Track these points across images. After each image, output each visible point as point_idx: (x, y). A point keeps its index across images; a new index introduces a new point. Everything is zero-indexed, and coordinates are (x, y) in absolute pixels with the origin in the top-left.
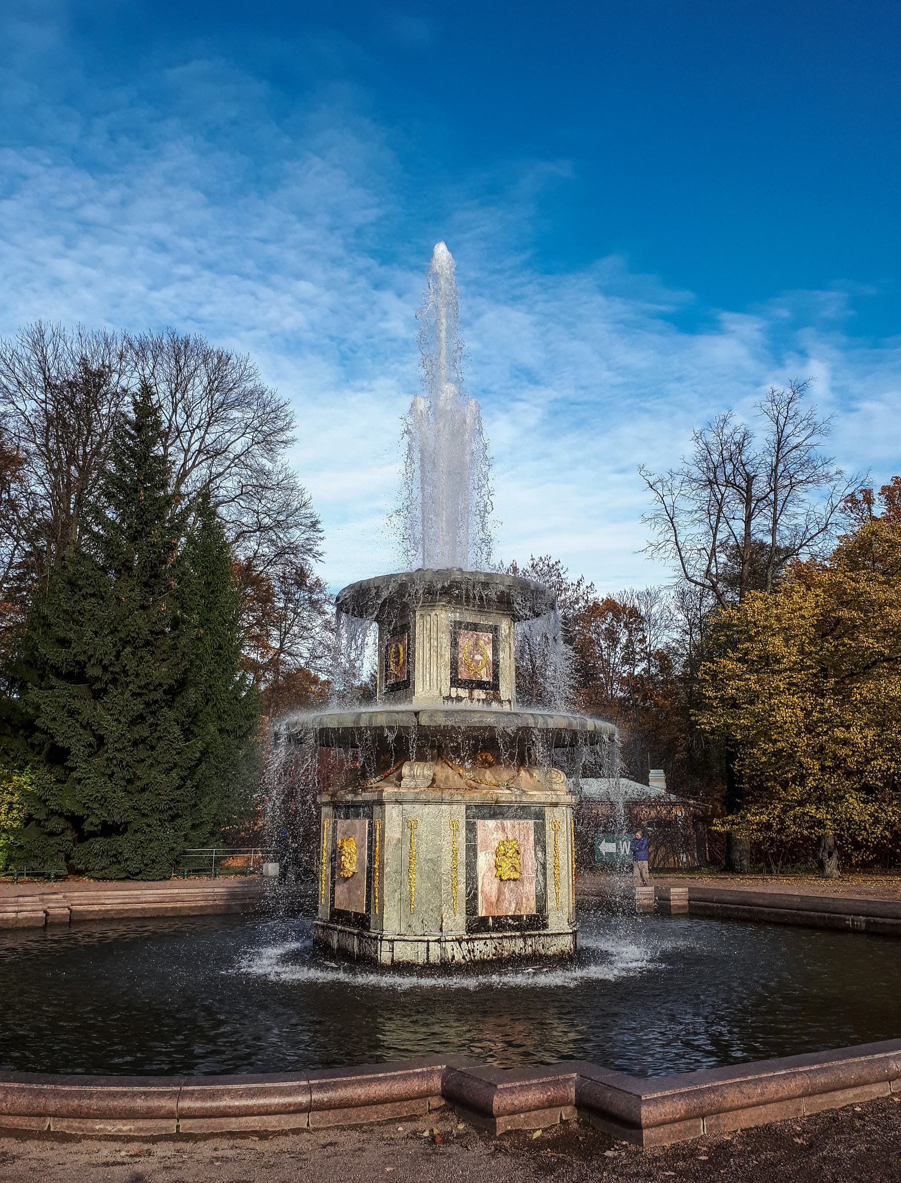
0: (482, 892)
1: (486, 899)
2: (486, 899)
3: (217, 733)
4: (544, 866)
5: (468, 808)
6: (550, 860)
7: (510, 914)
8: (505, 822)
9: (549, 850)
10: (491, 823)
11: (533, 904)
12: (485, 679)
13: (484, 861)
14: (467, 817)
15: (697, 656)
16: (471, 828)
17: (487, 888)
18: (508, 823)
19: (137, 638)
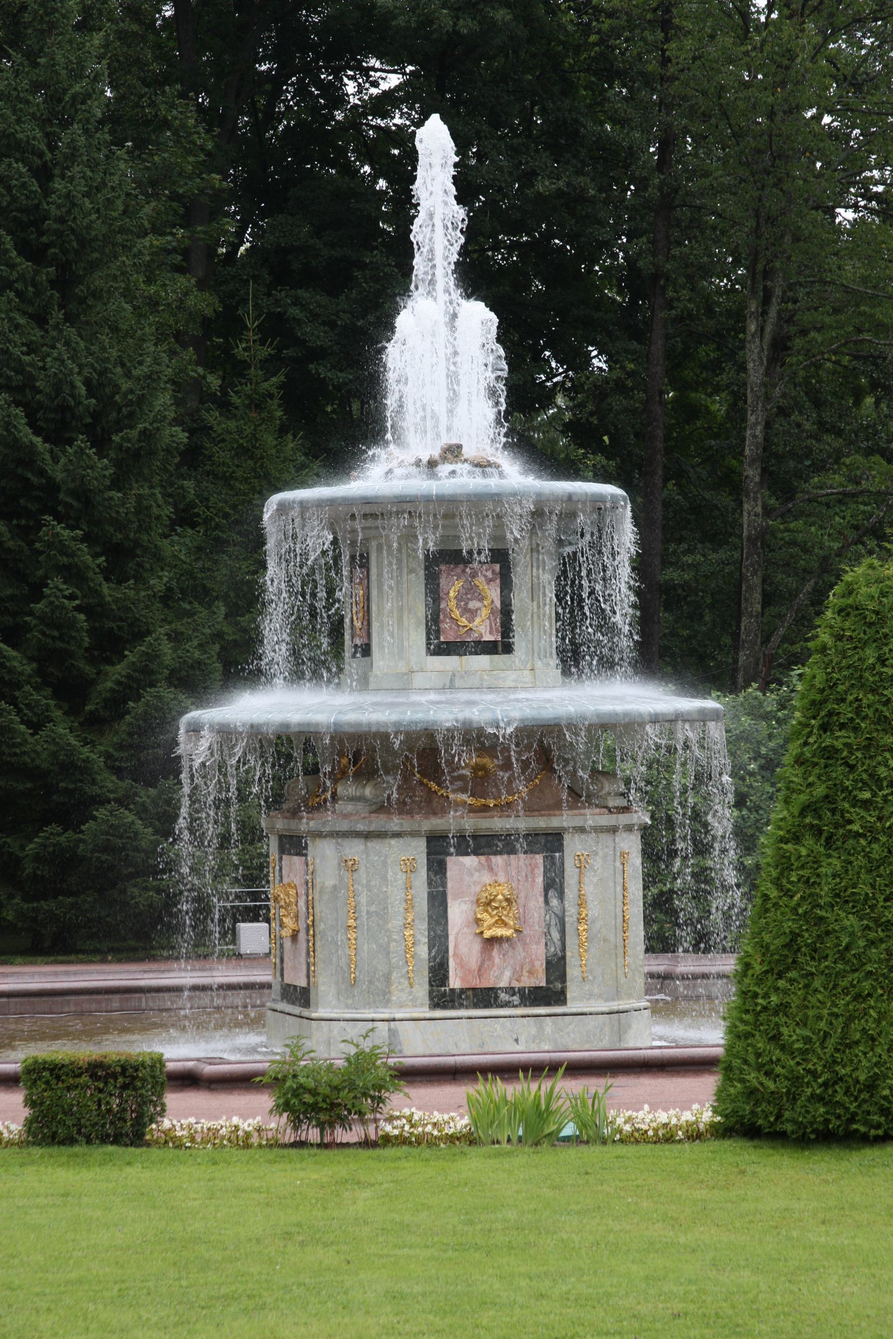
0: (455, 955)
1: (461, 965)
6: (571, 911)
7: (503, 984)
8: (493, 858)
9: (570, 893)
11: (540, 966)
12: (487, 638)
17: (463, 950)
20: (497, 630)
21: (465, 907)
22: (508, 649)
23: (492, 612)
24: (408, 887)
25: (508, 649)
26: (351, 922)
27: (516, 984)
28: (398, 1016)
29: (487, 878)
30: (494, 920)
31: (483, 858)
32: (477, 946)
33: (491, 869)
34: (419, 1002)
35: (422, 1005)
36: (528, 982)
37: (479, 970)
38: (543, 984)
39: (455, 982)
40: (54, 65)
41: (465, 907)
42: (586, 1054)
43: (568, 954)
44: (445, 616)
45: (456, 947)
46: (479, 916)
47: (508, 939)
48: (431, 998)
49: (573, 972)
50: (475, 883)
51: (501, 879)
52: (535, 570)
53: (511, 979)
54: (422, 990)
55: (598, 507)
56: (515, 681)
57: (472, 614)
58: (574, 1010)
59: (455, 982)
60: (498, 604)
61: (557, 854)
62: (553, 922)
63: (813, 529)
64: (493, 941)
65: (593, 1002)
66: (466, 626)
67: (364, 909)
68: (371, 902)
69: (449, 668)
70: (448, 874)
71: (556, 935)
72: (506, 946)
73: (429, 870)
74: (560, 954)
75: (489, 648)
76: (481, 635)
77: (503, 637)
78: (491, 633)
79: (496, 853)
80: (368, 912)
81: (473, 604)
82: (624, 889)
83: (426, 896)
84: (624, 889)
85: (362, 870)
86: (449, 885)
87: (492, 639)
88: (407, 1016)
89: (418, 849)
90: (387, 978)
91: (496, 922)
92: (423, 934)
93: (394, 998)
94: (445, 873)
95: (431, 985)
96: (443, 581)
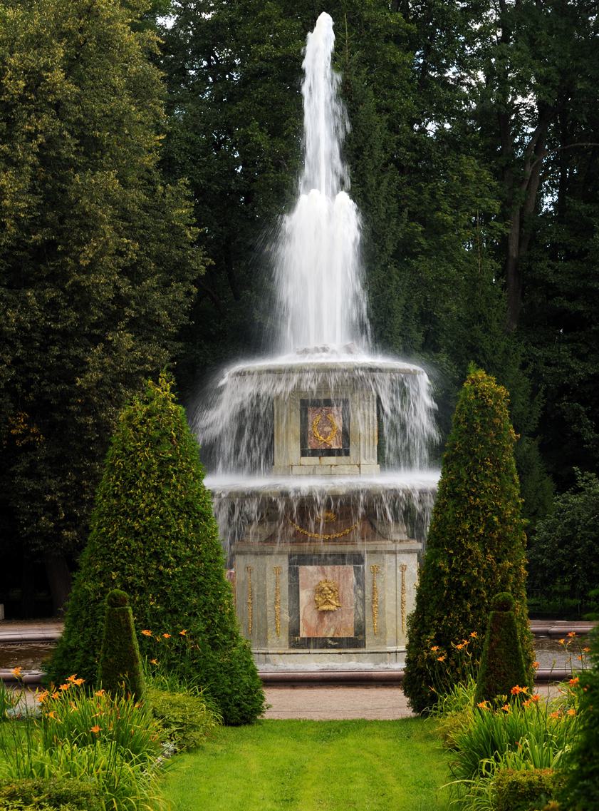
0: (303, 619)
1: (306, 624)
2: (306, 624)
3: (503, 349)
4: (363, 600)
5: (290, 557)
6: (368, 596)
7: (330, 636)
8: (325, 567)
9: (368, 587)
10: (311, 568)
11: (351, 626)
12: (335, 447)
13: (305, 596)
14: (290, 564)
15: (46, 479)
16: (294, 573)
17: (308, 617)
18: (328, 568)
19: (190, 803)
20: (340, 443)
21: (308, 593)
22: (347, 453)
23: (338, 433)
24: (277, 582)
25: (347, 453)
26: (249, 601)
27: (336, 636)
28: (270, 652)
29: (321, 578)
30: (324, 601)
31: (319, 567)
32: (316, 615)
33: (324, 573)
34: (283, 644)
35: (285, 646)
36: (343, 635)
37: (317, 628)
38: (353, 636)
39: (303, 634)
40: (478, 382)
41: (308, 593)
42: (393, 673)
43: (367, 620)
44: (311, 436)
45: (304, 614)
46: (316, 599)
47: (332, 611)
48: (290, 643)
49: (369, 630)
50: (315, 580)
51: (330, 578)
52: (366, 411)
53: (334, 632)
54: (284, 638)
55: (413, 375)
56: (349, 471)
57: (326, 435)
58: (369, 651)
59: (303, 634)
60: (341, 429)
61: (361, 566)
62: (359, 603)
63: (389, 267)
64: (324, 612)
65: (379, 647)
66: (322, 441)
67: (256, 593)
68: (258, 590)
69: (313, 463)
70: (300, 575)
71: (360, 610)
72: (331, 615)
73: (289, 573)
74: (362, 620)
75: (338, 453)
76: (331, 446)
77: (344, 446)
78: (337, 444)
79: (328, 564)
80: (258, 596)
81: (327, 429)
82: (403, 585)
83: (287, 586)
84: (403, 585)
85: (255, 572)
86: (300, 582)
87: (337, 448)
88: (276, 652)
89: (284, 563)
90: (266, 630)
91: (325, 602)
92: (285, 608)
93: (269, 642)
94: (298, 576)
95: (289, 635)
96: (310, 416)
